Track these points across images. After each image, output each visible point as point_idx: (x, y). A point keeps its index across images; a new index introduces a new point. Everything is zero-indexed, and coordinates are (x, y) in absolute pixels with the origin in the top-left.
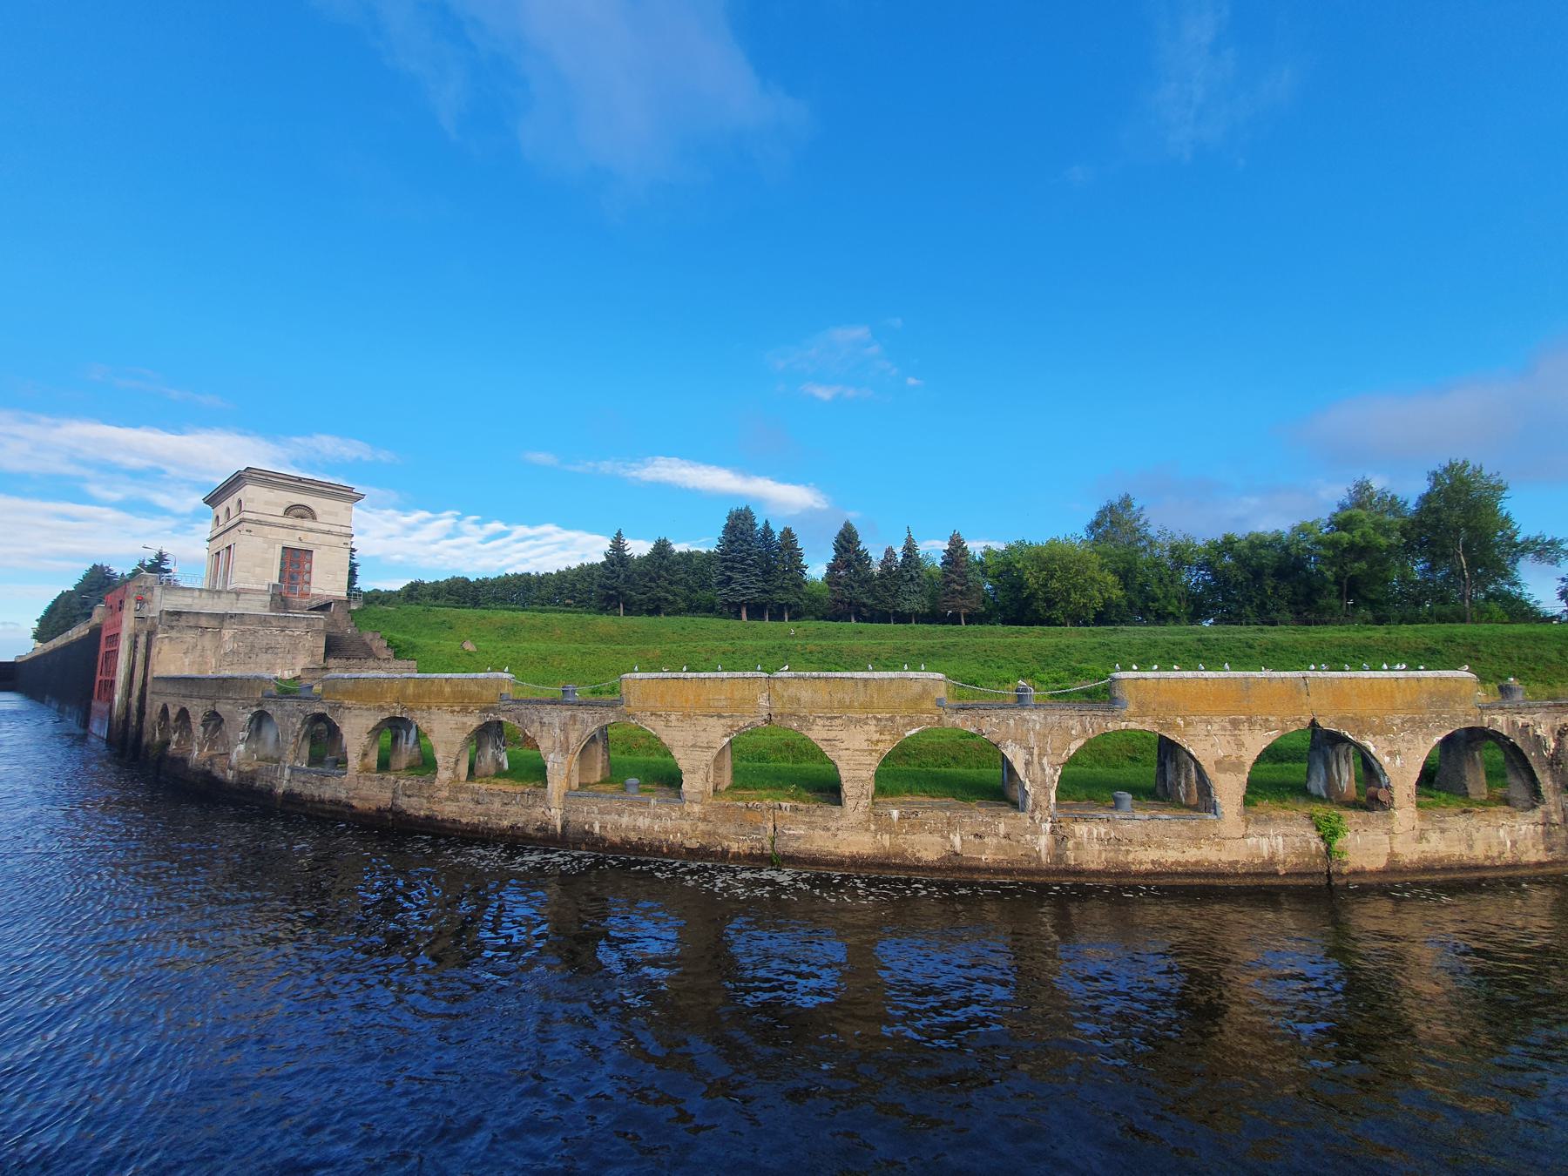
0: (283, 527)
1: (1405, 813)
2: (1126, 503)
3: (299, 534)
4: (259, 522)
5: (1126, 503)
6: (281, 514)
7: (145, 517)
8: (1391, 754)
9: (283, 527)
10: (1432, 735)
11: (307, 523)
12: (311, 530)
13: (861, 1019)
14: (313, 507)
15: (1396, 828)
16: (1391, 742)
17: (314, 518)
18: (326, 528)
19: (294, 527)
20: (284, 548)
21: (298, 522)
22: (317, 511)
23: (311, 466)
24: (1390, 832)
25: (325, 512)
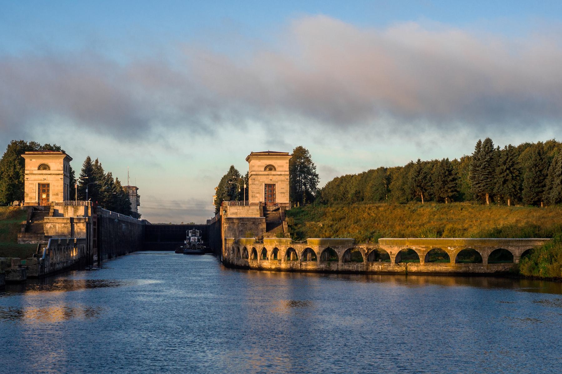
0: (264, 175)
1: (340, 262)
2: (510, 145)
3: (271, 177)
4: (257, 175)
5: (510, 145)
6: (263, 170)
7: (64, 184)
8: (339, 252)
9: (264, 175)
10: (345, 249)
11: (273, 172)
12: (274, 175)
13: (379, 274)
14: (274, 165)
15: (339, 264)
16: (339, 250)
17: (275, 170)
18: (279, 173)
19: (268, 175)
20: (265, 184)
21: (269, 172)
22: (276, 167)
23: (42, 156)
24: (338, 265)
25: (279, 166)
